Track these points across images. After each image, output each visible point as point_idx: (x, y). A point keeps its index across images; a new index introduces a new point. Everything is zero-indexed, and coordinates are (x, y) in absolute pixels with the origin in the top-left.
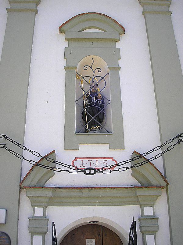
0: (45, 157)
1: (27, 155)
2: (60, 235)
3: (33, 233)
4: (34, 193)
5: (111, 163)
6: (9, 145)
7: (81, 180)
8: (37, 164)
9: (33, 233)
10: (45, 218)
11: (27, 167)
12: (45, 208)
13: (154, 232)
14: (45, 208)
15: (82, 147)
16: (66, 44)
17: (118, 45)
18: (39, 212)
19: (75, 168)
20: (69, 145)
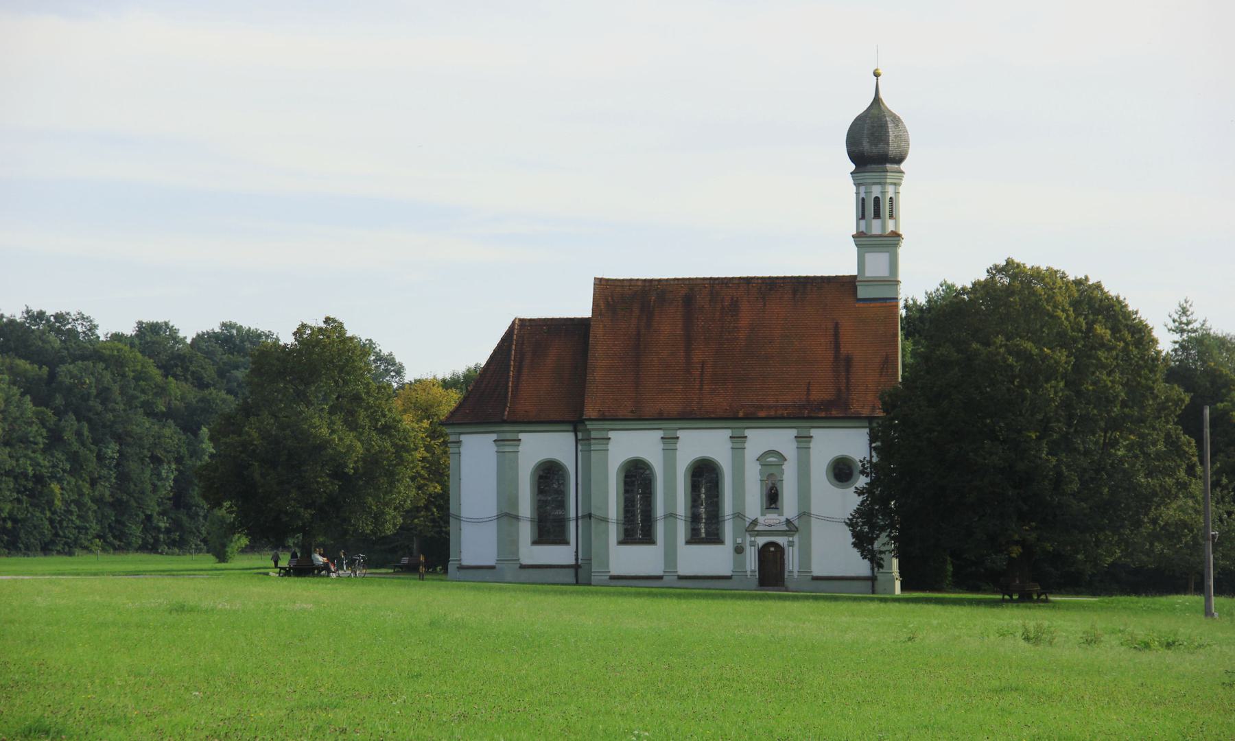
0: (754, 521)
1: (746, 519)
2: (760, 547)
3: (751, 546)
4: (751, 533)
5: (778, 521)
6: (740, 515)
7: (767, 528)
8: (751, 523)
9: (751, 546)
10: (755, 541)
11: (747, 524)
12: (1197, 456)
13: (792, 546)
14: (1197, 456)
15: (767, 515)
16: (760, 467)
17: (783, 467)
18: (753, 539)
19: (575, 516)
20: (763, 514)
